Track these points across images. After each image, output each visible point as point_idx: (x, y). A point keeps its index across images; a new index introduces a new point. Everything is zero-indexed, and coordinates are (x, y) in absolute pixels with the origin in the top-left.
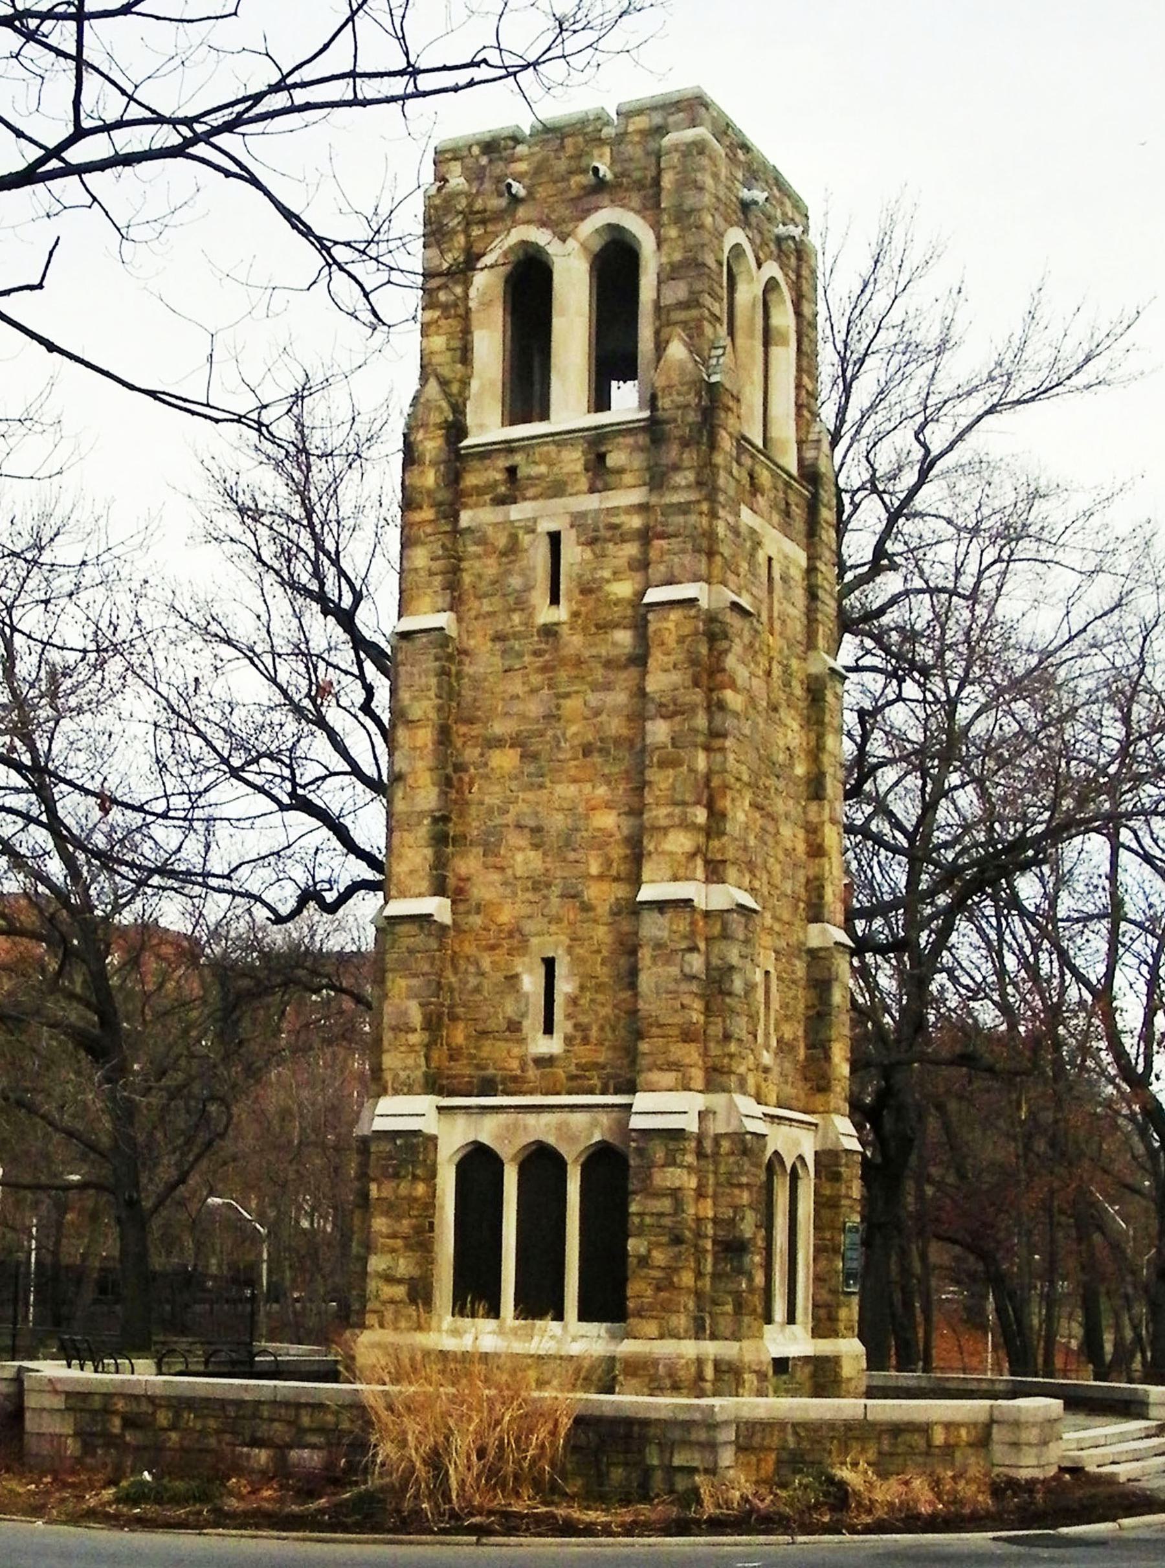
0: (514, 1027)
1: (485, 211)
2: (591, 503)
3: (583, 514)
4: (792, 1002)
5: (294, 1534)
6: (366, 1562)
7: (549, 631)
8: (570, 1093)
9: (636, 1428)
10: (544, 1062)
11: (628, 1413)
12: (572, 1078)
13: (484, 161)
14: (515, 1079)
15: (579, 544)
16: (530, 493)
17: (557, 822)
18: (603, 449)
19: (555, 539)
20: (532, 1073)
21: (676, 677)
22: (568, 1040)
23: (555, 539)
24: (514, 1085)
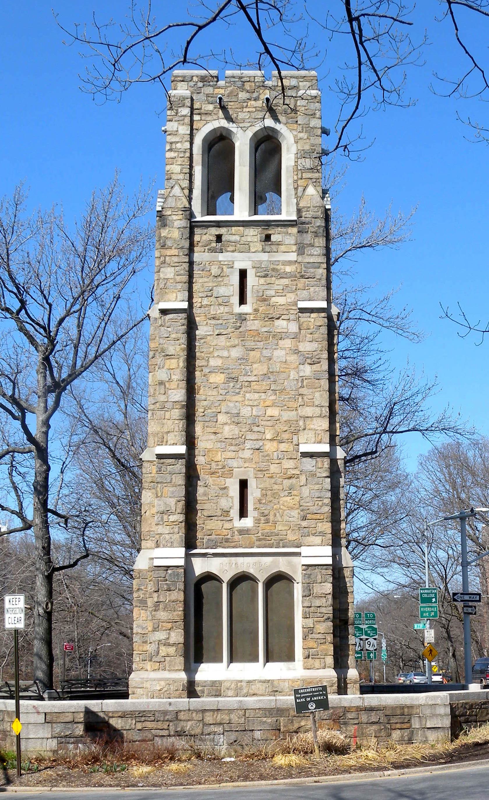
0: (226, 513)
1: (201, 109)
2: (265, 257)
3: (261, 262)
4: (150, 603)
5: (209, 797)
6: (85, 796)
7: (242, 318)
8: (259, 547)
9: (406, 710)
10: (242, 532)
11: (401, 703)
12: (259, 540)
13: (200, 84)
14: (227, 540)
15: (256, 276)
16: (230, 248)
17: (246, 411)
18: (270, 232)
19: (243, 274)
20: (237, 537)
21: (314, 346)
22: (257, 521)
23: (243, 274)
24: (226, 542)
